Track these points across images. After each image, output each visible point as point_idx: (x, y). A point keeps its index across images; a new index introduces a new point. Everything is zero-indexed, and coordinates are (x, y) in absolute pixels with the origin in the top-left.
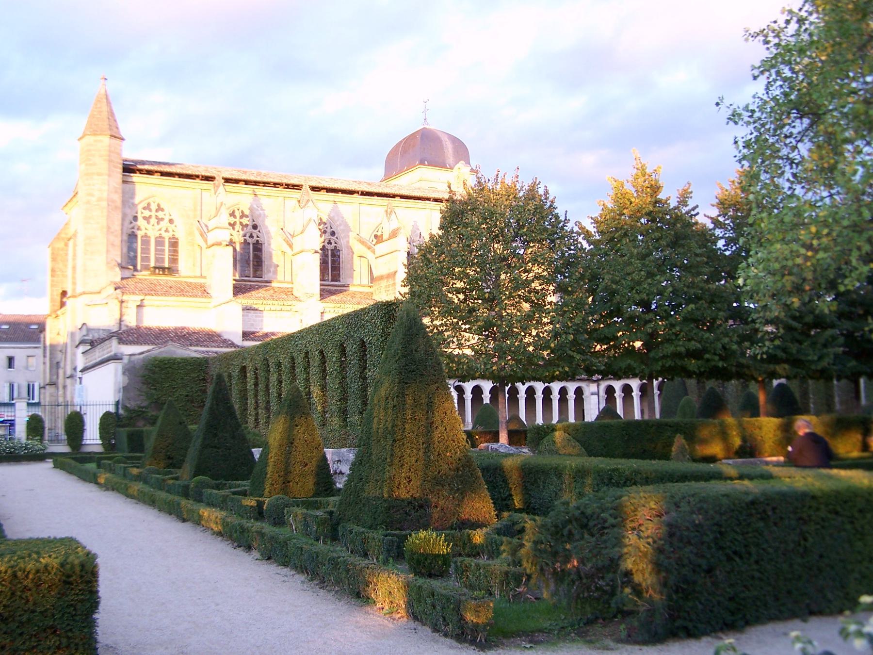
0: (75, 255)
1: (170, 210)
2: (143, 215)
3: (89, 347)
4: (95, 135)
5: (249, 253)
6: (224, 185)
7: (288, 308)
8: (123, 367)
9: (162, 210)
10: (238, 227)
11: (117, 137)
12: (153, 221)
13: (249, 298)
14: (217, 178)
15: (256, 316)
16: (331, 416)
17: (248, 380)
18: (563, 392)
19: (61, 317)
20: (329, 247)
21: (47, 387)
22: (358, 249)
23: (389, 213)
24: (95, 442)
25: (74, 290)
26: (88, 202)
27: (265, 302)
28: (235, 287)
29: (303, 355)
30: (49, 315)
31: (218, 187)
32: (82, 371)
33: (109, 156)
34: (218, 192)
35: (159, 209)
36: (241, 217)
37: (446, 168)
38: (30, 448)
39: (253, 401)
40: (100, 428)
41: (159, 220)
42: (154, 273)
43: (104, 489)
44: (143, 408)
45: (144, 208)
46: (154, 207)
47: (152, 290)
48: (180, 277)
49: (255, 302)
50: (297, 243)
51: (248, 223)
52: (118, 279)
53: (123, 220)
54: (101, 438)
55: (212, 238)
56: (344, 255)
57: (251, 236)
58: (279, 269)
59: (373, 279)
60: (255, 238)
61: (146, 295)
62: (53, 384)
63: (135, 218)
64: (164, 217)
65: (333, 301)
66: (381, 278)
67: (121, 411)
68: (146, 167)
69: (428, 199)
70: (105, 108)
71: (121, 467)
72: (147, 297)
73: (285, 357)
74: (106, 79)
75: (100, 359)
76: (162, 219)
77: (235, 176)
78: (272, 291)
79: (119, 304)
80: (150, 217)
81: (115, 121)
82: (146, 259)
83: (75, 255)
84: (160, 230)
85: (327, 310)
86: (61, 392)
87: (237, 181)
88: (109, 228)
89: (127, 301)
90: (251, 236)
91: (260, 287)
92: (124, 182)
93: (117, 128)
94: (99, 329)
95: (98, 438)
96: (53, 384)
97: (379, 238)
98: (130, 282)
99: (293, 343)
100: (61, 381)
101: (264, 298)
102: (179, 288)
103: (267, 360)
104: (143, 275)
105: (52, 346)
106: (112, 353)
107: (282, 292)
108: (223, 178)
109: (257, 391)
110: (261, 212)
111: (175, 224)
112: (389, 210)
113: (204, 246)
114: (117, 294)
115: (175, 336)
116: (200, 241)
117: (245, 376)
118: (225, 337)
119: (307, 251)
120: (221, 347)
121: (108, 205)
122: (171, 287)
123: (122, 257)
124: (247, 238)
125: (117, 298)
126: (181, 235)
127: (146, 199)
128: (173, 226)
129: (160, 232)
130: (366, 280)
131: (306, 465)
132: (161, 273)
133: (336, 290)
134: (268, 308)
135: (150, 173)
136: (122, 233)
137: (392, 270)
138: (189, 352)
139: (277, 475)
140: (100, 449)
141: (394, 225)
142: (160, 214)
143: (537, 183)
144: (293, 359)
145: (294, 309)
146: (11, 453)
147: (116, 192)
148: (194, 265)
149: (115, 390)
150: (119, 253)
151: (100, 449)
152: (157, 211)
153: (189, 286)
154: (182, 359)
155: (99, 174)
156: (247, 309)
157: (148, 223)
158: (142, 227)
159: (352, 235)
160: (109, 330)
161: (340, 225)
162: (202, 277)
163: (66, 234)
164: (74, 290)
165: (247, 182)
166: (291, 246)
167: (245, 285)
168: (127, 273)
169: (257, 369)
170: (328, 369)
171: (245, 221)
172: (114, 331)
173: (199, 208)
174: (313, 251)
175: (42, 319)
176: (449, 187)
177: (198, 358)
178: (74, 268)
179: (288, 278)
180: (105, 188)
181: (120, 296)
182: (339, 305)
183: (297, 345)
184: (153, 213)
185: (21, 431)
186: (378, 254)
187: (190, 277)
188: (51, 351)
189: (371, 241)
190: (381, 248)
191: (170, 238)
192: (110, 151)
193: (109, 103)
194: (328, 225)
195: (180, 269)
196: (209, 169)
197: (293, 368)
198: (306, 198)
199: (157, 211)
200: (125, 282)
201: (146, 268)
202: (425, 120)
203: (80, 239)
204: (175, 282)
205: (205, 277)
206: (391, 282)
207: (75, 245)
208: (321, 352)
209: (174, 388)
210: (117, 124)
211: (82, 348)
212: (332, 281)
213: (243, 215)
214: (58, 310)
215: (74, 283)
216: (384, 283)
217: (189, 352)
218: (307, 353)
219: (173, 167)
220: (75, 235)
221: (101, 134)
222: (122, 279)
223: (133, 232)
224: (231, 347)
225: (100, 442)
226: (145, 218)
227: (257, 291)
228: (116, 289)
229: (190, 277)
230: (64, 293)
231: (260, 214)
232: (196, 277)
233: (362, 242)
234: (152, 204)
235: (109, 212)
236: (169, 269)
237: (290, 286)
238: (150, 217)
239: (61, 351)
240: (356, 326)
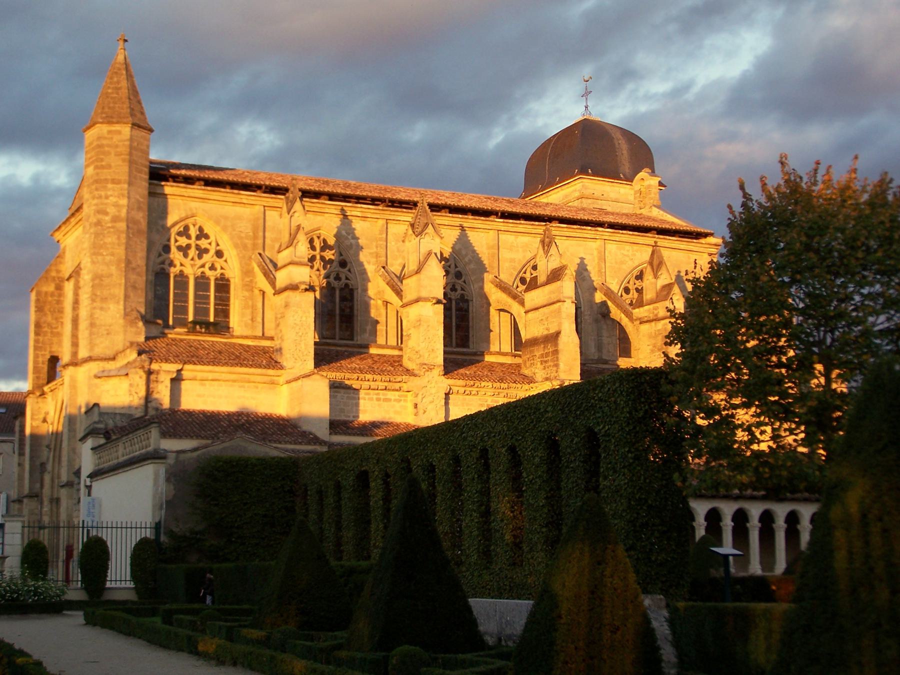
0: (76, 302)
1: (219, 237)
2: (177, 244)
3: (102, 441)
4: (110, 123)
5: (334, 302)
6: (301, 200)
7: (397, 386)
8: (166, 472)
9: (207, 237)
10: (318, 264)
11: (141, 126)
12: (192, 252)
13: (339, 370)
14: (292, 189)
15: (348, 397)
16: (531, 550)
17: (372, 493)
18: (767, 518)
19: (49, 397)
20: (454, 296)
21: (25, 500)
22: (495, 296)
23: (547, 244)
24: (123, 585)
25: (75, 354)
26: (98, 223)
27: (362, 376)
28: (316, 354)
29: (476, 454)
30: (30, 393)
31: (293, 202)
32: (92, 476)
33: (130, 154)
34: (292, 211)
35: (202, 235)
36: (323, 249)
37: (620, 179)
38: (41, 594)
39: (381, 526)
40: (132, 565)
41: (202, 252)
42: (193, 331)
43: (213, 662)
44: (197, 533)
45: (180, 234)
46: (193, 232)
47: (194, 356)
48: (233, 337)
49: (347, 375)
50: (410, 287)
51: (333, 257)
52: (141, 339)
53: (149, 250)
54: (134, 577)
55: (282, 277)
56: (474, 308)
57: (338, 278)
58: (379, 327)
59: (518, 343)
60: (344, 280)
61: (185, 363)
62: (35, 496)
63: (167, 249)
64: (208, 246)
65: (464, 377)
66: (534, 342)
67: (163, 538)
68: (183, 172)
69: (601, 224)
70: (124, 84)
71: (220, 627)
72: (187, 367)
73: (442, 458)
74: (126, 41)
75: (126, 458)
76: (206, 251)
77: (315, 187)
78: (370, 360)
79: (144, 376)
80: (188, 247)
81: (139, 102)
82: (182, 310)
83: (76, 302)
84: (203, 266)
85: (455, 389)
86: (46, 509)
87: (317, 195)
88: (128, 262)
89: (158, 372)
90: (338, 278)
91: (350, 355)
92: (152, 194)
93: (142, 113)
94: (116, 414)
95: (128, 578)
96: (35, 496)
97: (532, 285)
98: (160, 343)
99: (457, 434)
100: (46, 491)
101: (361, 371)
102: (233, 353)
103: (409, 462)
104: (178, 333)
105: (35, 437)
106: (150, 449)
107: (385, 362)
108: (300, 190)
109: (388, 510)
110: (353, 241)
111: (224, 259)
112: (547, 240)
113: (269, 290)
114: (141, 360)
115: (229, 426)
116: (262, 282)
117: (367, 486)
118: (305, 428)
119: (426, 300)
120: (300, 443)
121: (128, 227)
122: (220, 352)
123: (146, 306)
124: (332, 279)
125: (143, 367)
126: (233, 272)
127: (181, 220)
128: (221, 261)
129: (202, 269)
130: (507, 347)
131: (618, 629)
132: (203, 330)
133: (465, 361)
134: (366, 384)
135: (189, 181)
136: (147, 270)
137: (552, 331)
138: (267, 450)
139: (573, 646)
140: (132, 596)
141: (554, 264)
142: (203, 243)
143: (887, 180)
144: (457, 460)
145: (405, 387)
146: (13, 600)
147: (139, 209)
148: (252, 320)
149: (154, 506)
150: (142, 300)
151: (132, 596)
152: (198, 238)
153: (247, 352)
154: (258, 459)
155: (117, 182)
156: (335, 387)
157: (186, 255)
158: (177, 263)
159: (488, 277)
160: (131, 415)
161: (470, 261)
162: (264, 337)
163: (58, 271)
164: (75, 354)
165: (332, 197)
166: (399, 293)
167: (329, 351)
168: (155, 331)
169: (387, 475)
170: (524, 475)
171: (329, 255)
172: (137, 416)
173: (261, 234)
174: (434, 301)
175: (20, 399)
176: (742, 187)
177: (281, 458)
178: (75, 321)
179: (392, 341)
180: (124, 202)
181: (146, 364)
182: (472, 383)
183: (465, 439)
184: (192, 242)
185: (13, 566)
186: (529, 304)
187: (246, 337)
188: (31, 446)
189: (515, 286)
190: (533, 298)
191: (216, 279)
192: (131, 147)
193: (129, 76)
194: (452, 262)
195: (231, 325)
196: (273, 177)
197: (456, 474)
198: (423, 220)
199: (198, 238)
200: (151, 343)
201: (181, 322)
202: (586, 107)
203: (86, 277)
204: (225, 344)
205: (272, 339)
206: (550, 349)
207: (77, 288)
208: (512, 450)
209: (245, 504)
210: (142, 108)
211: (90, 443)
212: (458, 346)
213: (325, 246)
214: (43, 385)
215: (75, 344)
216: (538, 351)
217: (267, 450)
218: (484, 453)
219: (222, 173)
220: (76, 272)
221: (118, 123)
222: (147, 338)
223: (163, 269)
224: (315, 444)
225: (132, 585)
226: (180, 248)
227: (348, 361)
228: (140, 354)
229: (246, 337)
230: (54, 360)
231: (351, 244)
232: (255, 338)
233: (502, 287)
234: (191, 227)
235: (128, 238)
236: (215, 324)
237: (396, 352)
238: (188, 247)
239: (48, 446)
240: (578, 408)
